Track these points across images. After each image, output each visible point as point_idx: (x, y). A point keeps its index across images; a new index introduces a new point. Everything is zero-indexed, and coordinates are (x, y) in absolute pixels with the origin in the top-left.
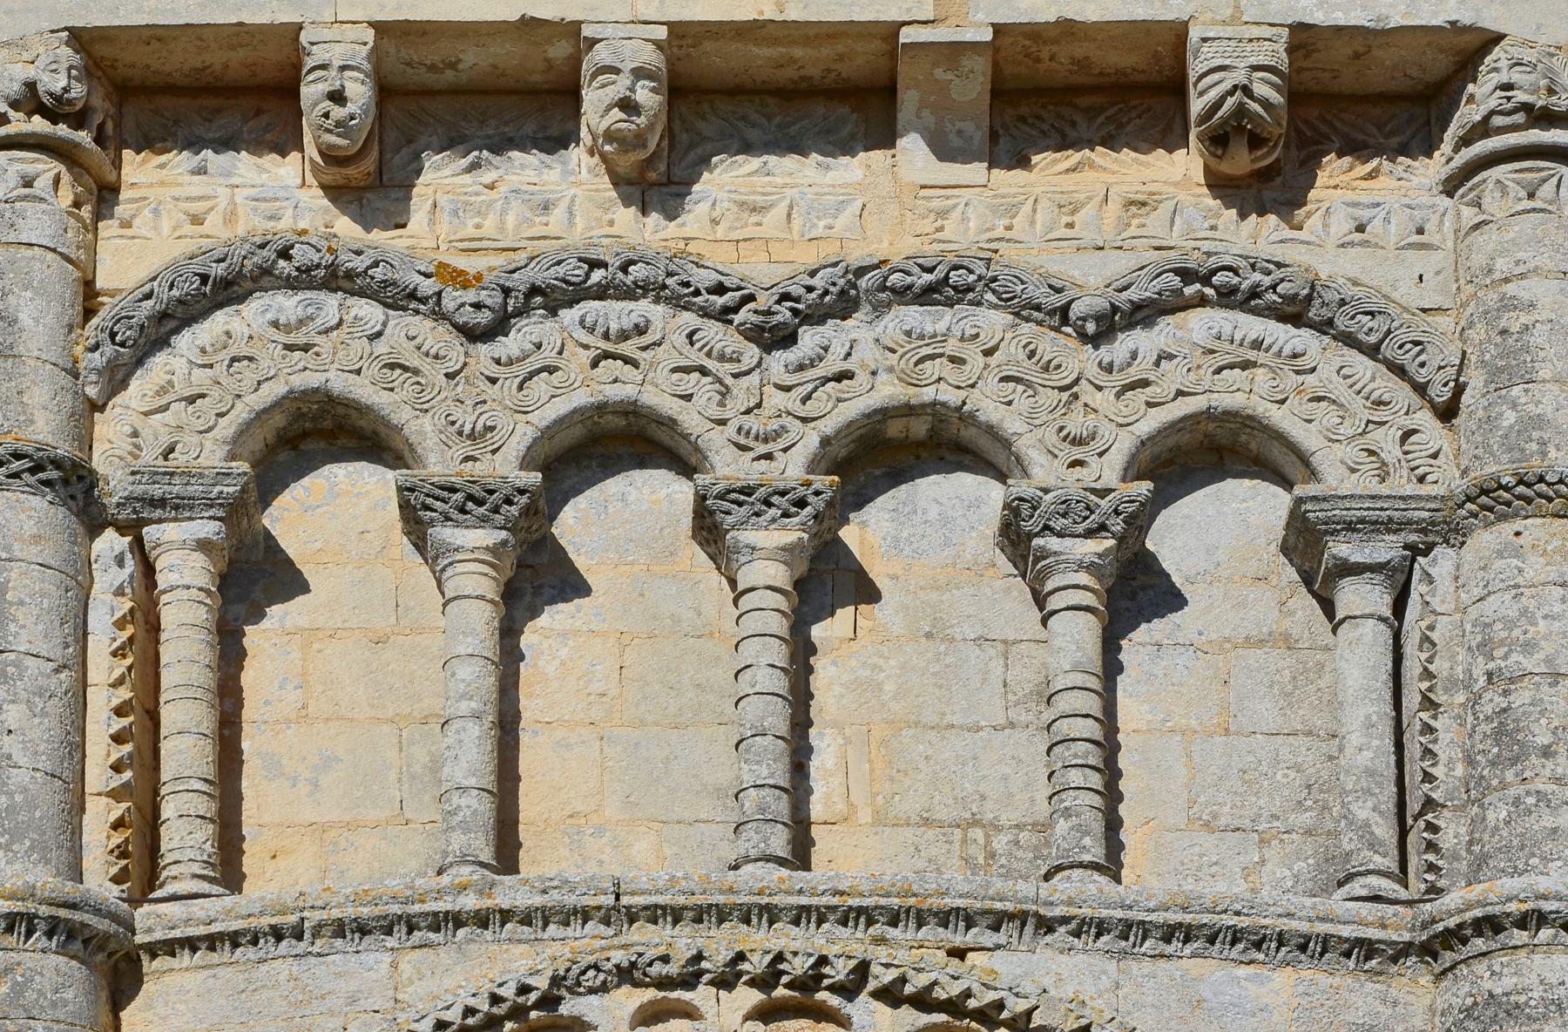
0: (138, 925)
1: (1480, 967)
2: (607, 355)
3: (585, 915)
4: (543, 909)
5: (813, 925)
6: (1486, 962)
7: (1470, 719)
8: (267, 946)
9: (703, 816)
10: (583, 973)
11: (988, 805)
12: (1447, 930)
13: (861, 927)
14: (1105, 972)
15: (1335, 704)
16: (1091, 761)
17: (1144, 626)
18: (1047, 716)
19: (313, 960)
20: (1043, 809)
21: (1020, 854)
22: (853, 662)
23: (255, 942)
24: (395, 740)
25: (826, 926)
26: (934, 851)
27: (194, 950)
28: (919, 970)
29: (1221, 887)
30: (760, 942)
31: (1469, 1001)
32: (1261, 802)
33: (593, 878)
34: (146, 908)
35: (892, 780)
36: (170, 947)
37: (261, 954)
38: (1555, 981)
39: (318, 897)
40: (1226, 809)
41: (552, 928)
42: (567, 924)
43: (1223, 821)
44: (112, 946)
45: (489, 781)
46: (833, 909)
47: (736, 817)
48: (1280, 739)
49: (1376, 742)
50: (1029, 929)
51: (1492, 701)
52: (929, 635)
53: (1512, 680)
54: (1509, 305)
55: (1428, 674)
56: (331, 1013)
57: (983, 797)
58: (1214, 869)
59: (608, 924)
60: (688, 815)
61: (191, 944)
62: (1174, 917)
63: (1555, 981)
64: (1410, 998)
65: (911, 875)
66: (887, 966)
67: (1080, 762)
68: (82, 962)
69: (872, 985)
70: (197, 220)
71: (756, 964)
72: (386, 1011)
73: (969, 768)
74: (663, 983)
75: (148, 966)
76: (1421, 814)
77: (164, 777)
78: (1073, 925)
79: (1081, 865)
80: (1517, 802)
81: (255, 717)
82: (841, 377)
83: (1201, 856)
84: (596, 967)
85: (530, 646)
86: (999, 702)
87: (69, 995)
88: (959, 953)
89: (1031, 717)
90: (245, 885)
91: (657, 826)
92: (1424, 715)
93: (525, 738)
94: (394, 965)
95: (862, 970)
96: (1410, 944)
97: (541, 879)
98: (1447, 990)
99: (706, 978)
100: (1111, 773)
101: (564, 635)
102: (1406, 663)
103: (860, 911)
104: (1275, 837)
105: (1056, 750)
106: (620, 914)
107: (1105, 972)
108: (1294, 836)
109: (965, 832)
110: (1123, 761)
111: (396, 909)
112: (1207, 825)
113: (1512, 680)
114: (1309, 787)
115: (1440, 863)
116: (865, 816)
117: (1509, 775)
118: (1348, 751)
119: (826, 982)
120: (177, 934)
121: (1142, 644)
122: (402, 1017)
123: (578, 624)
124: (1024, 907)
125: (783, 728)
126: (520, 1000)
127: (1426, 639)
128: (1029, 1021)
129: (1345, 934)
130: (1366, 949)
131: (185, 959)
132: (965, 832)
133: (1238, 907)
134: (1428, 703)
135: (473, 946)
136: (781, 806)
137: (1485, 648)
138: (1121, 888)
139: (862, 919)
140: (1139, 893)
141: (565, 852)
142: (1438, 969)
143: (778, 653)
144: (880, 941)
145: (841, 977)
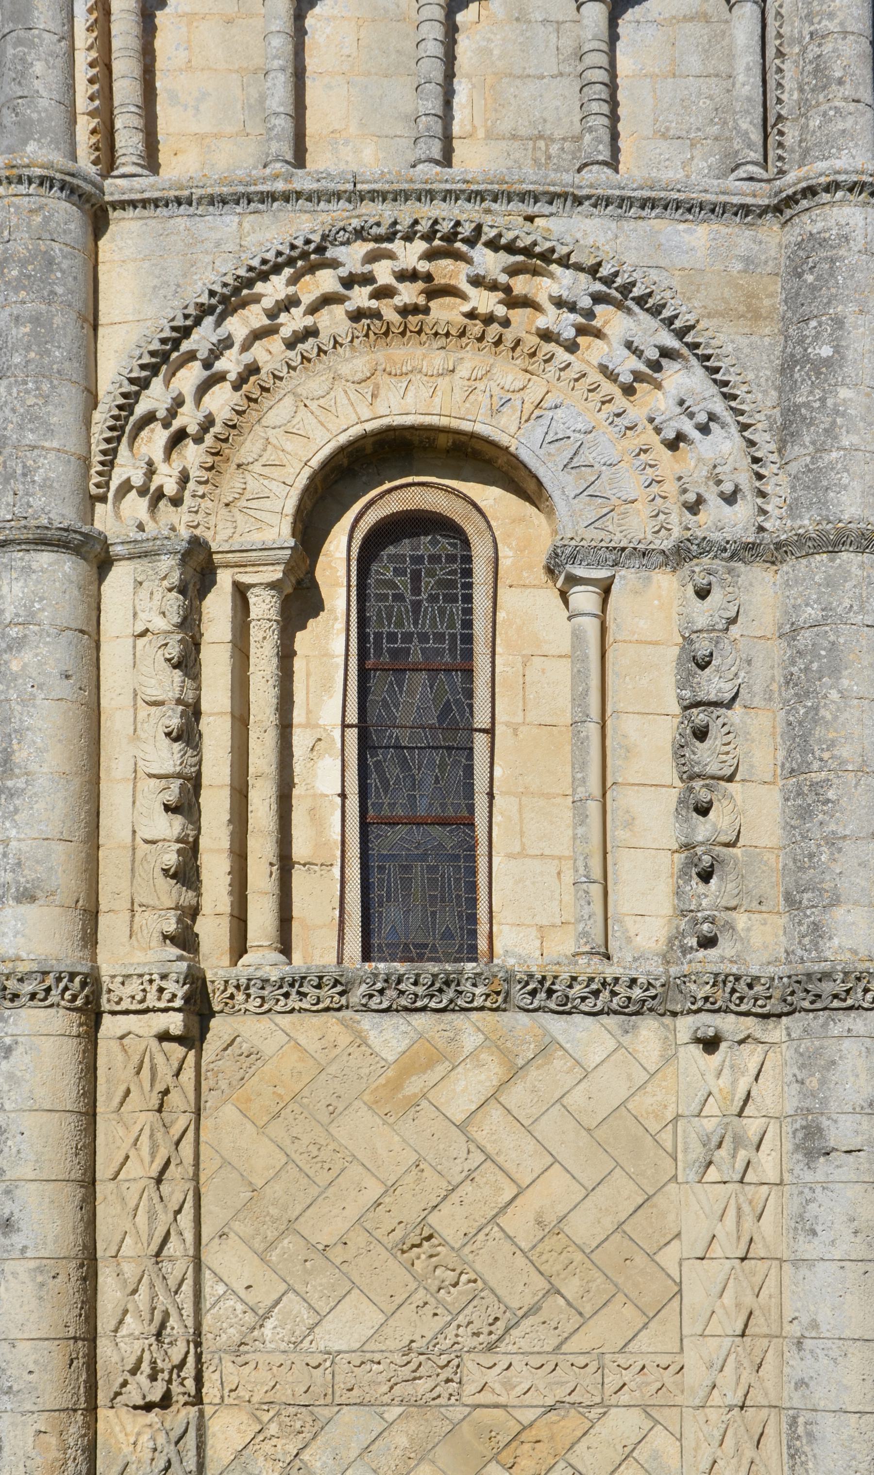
0: (106, 190)
1: (805, 217)
3: (338, 195)
4: (317, 191)
5: (453, 202)
6: (808, 214)
7: (801, 62)
8: (173, 207)
9: (398, 133)
10: (338, 233)
11: (548, 126)
12: (788, 196)
13: (478, 202)
14: (609, 229)
15: (730, 57)
16: (603, 96)
17: (630, 10)
18: (580, 69)
19: (197, 219)
20: (577, 127)
21: (564, 156)
22: (478, 37)
23: (167, 205)
24: (239, 83)
25: (459, 202)
26: (517, 155)
27: (135, 207)
28: (509, 229)
29: (670, 174)
30: (428, 211)
31: (800, 238)
32: (692, 120)
33: (343, 172)
34: (110, 181)
35: (496, 110)
36: (123, 205)
37: (170, 213)
38: (844, 223)
39: (200, 180)
40: (674, 125)
41: (322, 203)
42: (329, 202)
43: (671, 133)
44: (93, 201)
45: (290, 109)
46: (463, 191)
47: (415, 134)
48: (702, 79)
49: (752, 80)
50: (569, 203)
51: (813, 50)
52: (517, 19)
53: (823, 37)
55: (779, 36)
56: (207, 253)
57: (545, 121)
58: (667, 163)
59: (350, 202)
60: (391, 133)
61: (133, 204)
62: (646, 194)
63: (844, 223)
64: (768, 239)
65: (505, 170)
66: (492, 227)
67: (597, 97)
68: (79, 208)
69: (484, 238)
71: (424, 227)
72: (235, 252)
73: (537, 103)
74: (378, 239)
75: (113, 215)
76: (775, 125)
77: (116, 103)
78: (593, 200)
79: (598, 163)
80: (825, 114)
81: (164, 67)
83: (660, 154)
84: (344, 229)
85: (310, 26)
86: (554, 60)
87: (72, 226)
88: (530, 219)
89: (571, 69)
90: (161, 171)
91: (375, 139)
92: (777, 61)
93: (308, 82)
94: (240, 224)
95: (478, 229)
96: (768, 206)
97: (316, 172)
98: (788, 232)
99: (399, 235)
100: (613, 103)
101: (328, 19)
102: (768, 29)
103: (477, 193)
104: (698, 142)
105: (585, 89)
106: (358, 197)
107: (609, 229)
108: (709, 141)
109: (535, 142)
110: (621, 96)
111: (241, 189)
112: (663, 135)
113: (823, 37)
114: (717, 109)
115: (785, 155)
116: (481, 133)
117: (821, 98)
118: (738, 86)
119: (460, 237)
120: (125, 197)
121: (630, 22)
122: (243, 256)
123: (336, 12)
124: (567, 189)
125: (440, 78)
126: (306, 248)
127: (778, 13)
128: (569, 259)
129: (735, 202)
130: (745, 210)
131: (130, 213)
132: (535, 142)
133: (679, 187)
134: (780, 54)
135: (281, 214)
136: (437, 127)
137: (809, 17)
138: (618, 176)
139: (478, 198)
140: (628, 179)
141: (329, 155)
142: (783, 220)
143: (437, 31)
144: (488, 211)
145: (467, 234)
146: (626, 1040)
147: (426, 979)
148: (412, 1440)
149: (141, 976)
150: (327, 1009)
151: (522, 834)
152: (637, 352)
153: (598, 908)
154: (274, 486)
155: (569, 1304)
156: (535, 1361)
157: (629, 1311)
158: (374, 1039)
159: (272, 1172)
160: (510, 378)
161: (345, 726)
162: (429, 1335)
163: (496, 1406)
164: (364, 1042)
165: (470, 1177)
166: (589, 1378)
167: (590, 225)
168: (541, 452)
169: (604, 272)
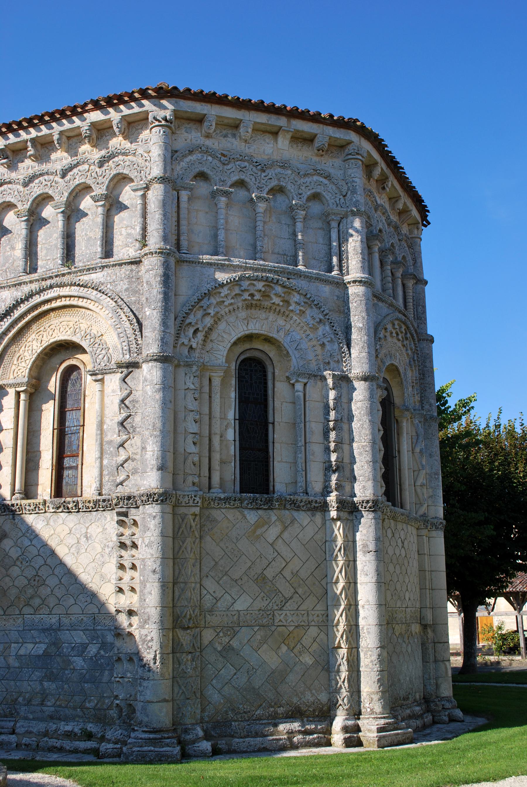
2: (241, 171)
54: (353, 181)
70: (186, 140)
82: (271, 179)
116: (270, 252)
146: (313, 518)
147: (263, 499)
148: (261, 637)
149: (188, 495)
150: (236, 507)
151: (281, 455)
152: (314, 319)
153: (304, 478)
154: (220, 347)
155: (300, 596)
156: (292, 613)
157: (315, 598)
158: (248, 517)
159: (221, 557)
160: (281, 322)
161: (235, 419)
162: (265, 605)
163: (283, 626)
164: (245, 517)
165: (274, 559)
166: (305, 618)
167: (303, 282)
168: (289, 344)
169: (308, 296)
